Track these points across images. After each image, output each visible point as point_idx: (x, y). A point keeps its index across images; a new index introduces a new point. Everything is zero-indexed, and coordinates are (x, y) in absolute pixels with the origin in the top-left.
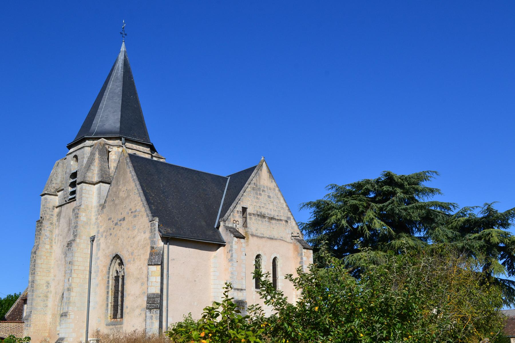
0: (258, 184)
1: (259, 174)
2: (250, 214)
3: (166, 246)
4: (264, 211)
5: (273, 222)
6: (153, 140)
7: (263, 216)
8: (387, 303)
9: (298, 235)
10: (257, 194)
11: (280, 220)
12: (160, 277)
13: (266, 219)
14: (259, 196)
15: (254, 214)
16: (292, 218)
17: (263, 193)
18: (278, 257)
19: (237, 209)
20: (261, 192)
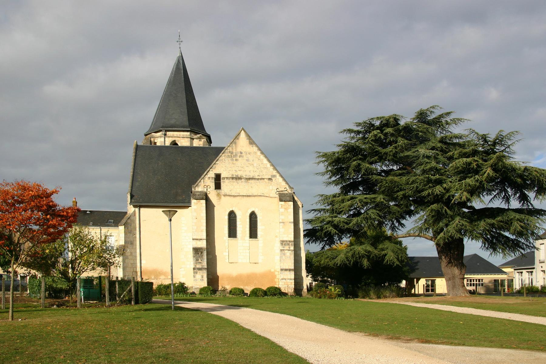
0: (234, 151)
1: (235, 143)
2: (224, 178)
3: (137, 210)
4: (240, 174)
5: (251, 181)
6: (208, 132)
7: (238, 178)
8: (54, 268)
9: (286, 189)
10: (232, 160)
11: (264, 179)
12: (292, 226)
13: (243, 180)
14: (235, 162)
15: (227, 178)
16: (278, 175)
17: (240, 159)
18: (256, 212)
19: (209, 176)
20: (238, 158)
